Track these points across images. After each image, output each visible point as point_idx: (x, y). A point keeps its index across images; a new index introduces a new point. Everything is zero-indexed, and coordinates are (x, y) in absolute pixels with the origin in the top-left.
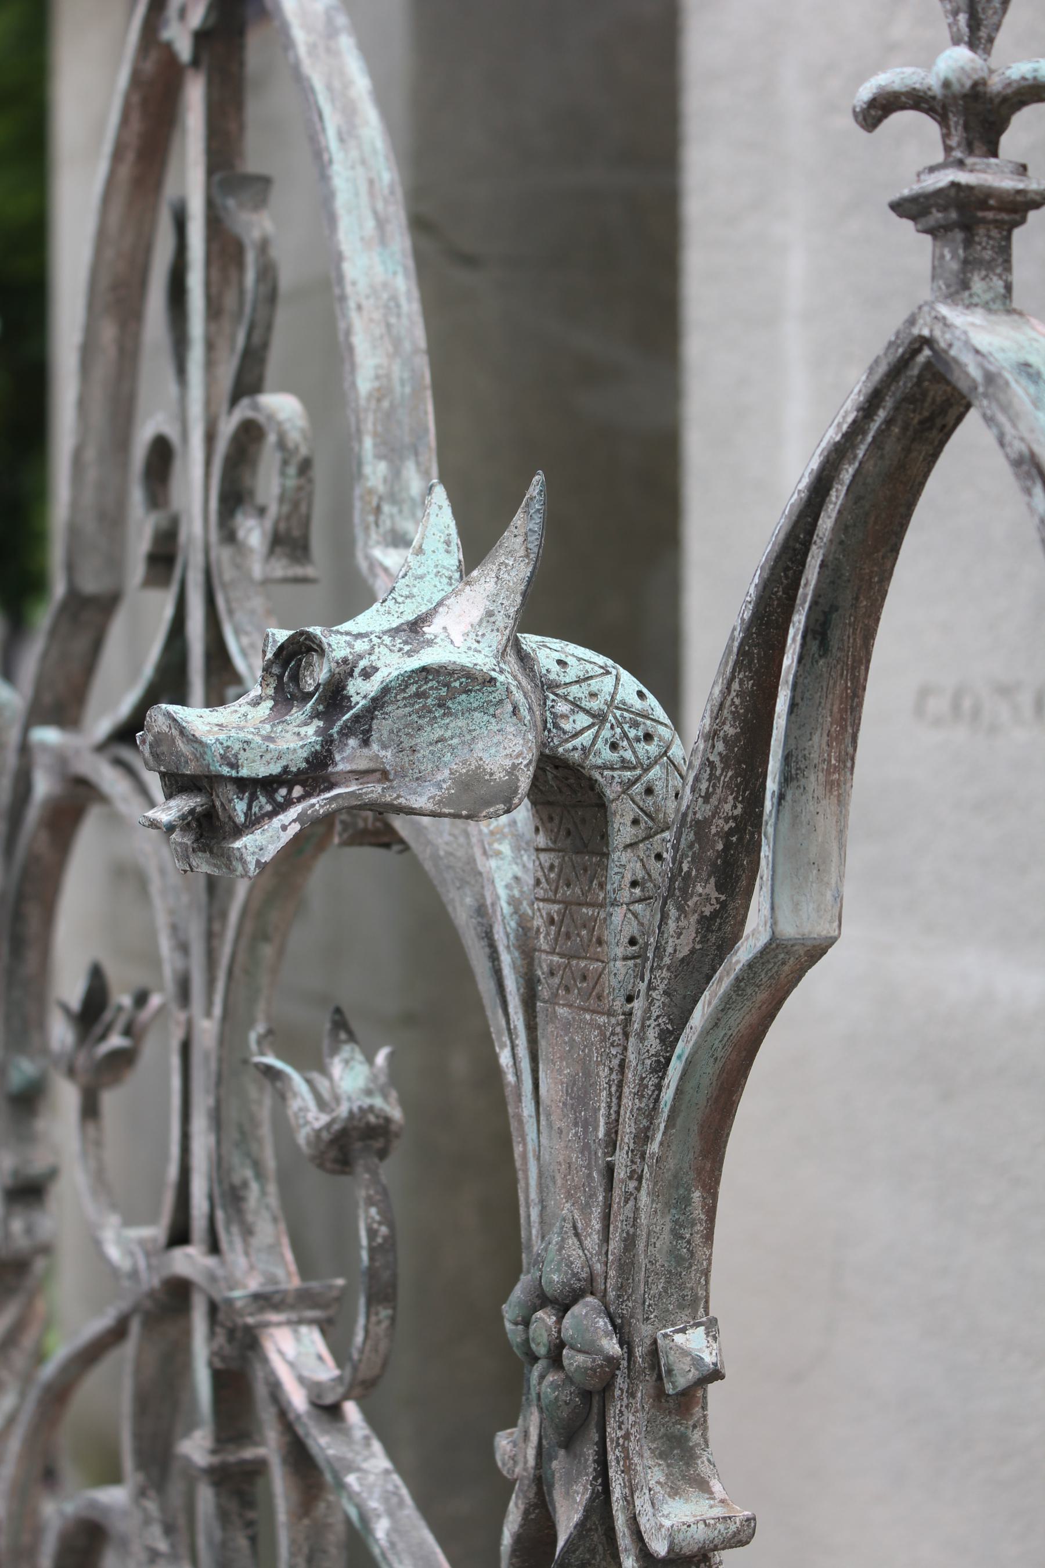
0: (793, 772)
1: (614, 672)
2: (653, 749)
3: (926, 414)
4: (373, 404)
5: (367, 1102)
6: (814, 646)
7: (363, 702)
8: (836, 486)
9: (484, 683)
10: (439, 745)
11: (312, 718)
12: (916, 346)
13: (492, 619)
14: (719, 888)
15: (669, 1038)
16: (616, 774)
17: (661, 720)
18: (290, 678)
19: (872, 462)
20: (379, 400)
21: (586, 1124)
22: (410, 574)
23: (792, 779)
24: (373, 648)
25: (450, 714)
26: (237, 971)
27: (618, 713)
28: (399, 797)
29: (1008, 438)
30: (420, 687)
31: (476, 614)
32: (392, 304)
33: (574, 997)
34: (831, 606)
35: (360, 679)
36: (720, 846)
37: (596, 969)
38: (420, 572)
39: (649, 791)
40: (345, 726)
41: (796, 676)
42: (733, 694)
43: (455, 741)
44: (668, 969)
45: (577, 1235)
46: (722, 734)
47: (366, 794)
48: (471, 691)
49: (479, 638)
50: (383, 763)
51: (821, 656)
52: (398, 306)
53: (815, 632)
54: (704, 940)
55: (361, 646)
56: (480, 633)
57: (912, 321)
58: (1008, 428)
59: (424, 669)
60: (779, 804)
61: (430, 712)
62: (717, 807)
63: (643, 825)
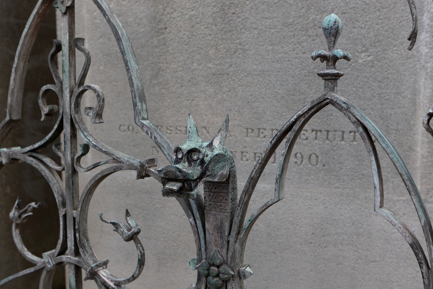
31: (218, 142)
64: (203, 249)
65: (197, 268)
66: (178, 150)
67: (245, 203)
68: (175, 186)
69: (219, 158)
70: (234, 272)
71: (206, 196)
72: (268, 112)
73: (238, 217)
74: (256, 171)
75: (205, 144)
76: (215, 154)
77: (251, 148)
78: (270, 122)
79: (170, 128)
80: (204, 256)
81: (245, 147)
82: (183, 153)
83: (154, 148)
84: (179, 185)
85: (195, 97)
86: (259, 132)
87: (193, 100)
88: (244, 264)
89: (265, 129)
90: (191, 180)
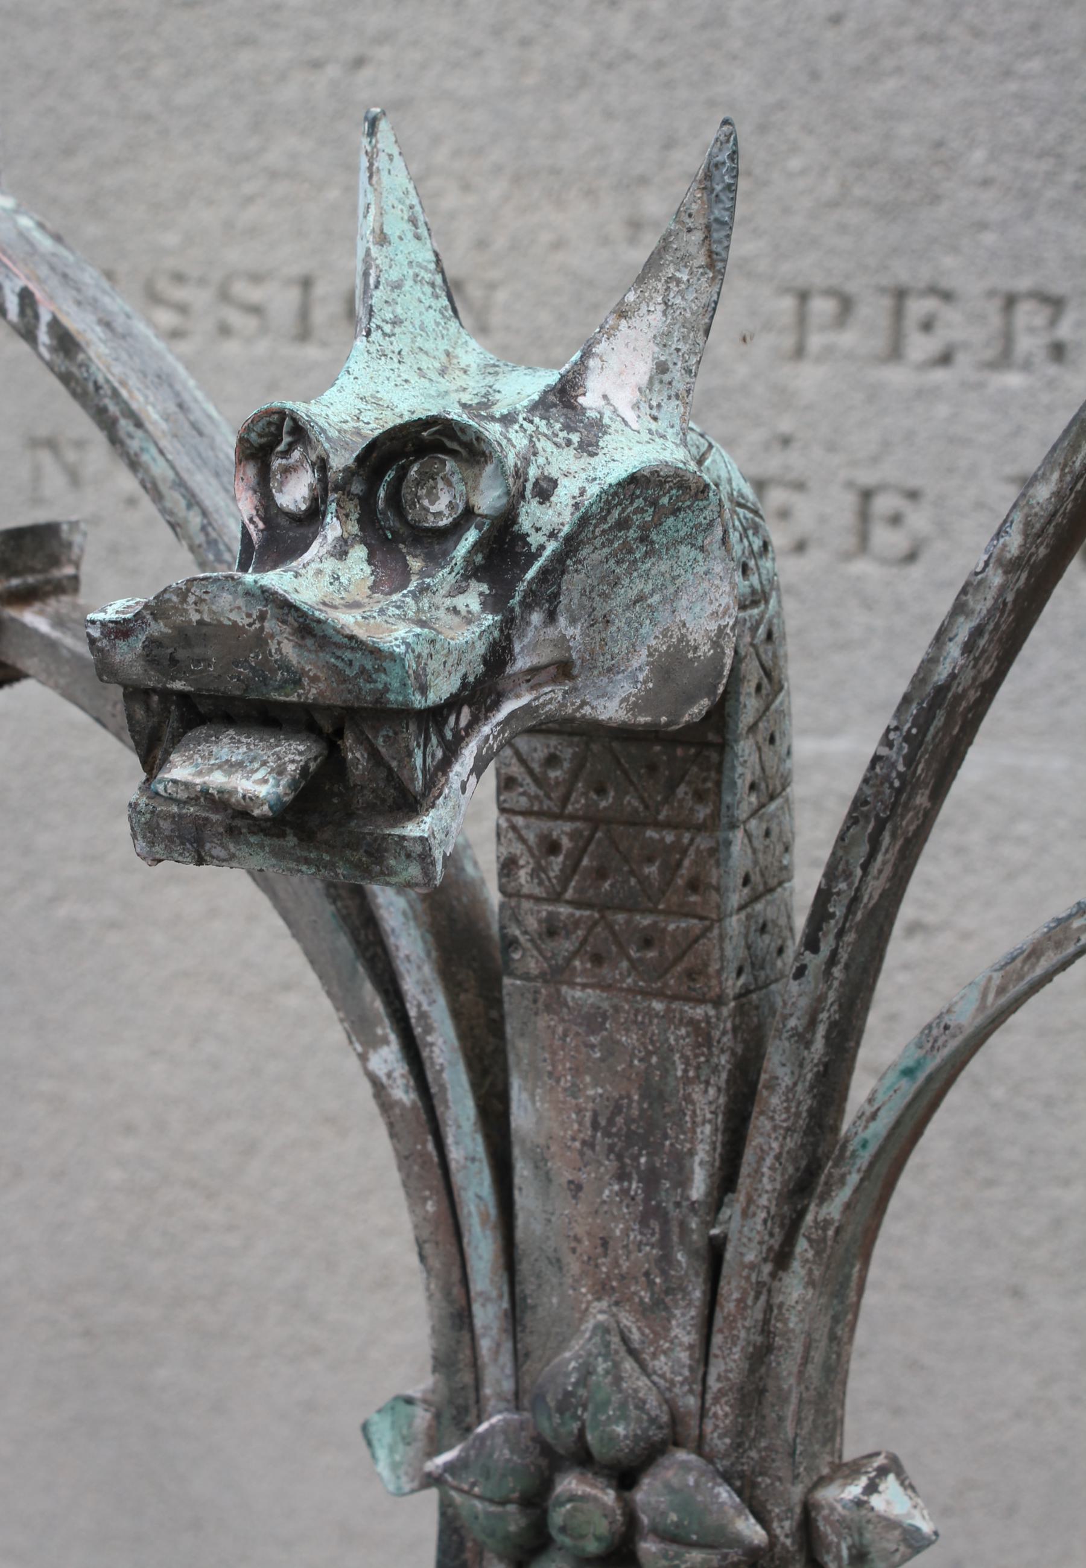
7: (551, 547)
9: (696, 494)
11: (466, 577)
13: (666, 378)
22: (382, 280)
28: (584, 703)
30: (623, 510)
31: (643, 370)
33: (619, 971)
35: (534, 503)
37: (686, 931)
40: (529, 592)
43: (656, 598)
45: (633, 1353)
47: (544, 705)
48: (679, 509)
49: (654, 412)
50: (570, 648)
56: (654, 403)
64: (487, 1316)
65: (431, 1480)
66: (272, 440)
67: (872, 914)
68: (253, 773)
69: (654, 505)
70: (763, 1520)
71: (518, 848)
72: (979, 155)
73: (803, 1038)
74: (977, 632)
75: (523, 386)
76: (618, 473)
77: (831, 447)
78: (989, 238)
79: (179, 294)
80: (497, 1377)
81: (786, 441)
82: (322, 466)
83: (45, 457)
84: (295, 753)
85: (384, 37)
86: (898, 314)
87: (359, 62)
88: (848, 1455)
89: (947, 296)
90: (405, 713)
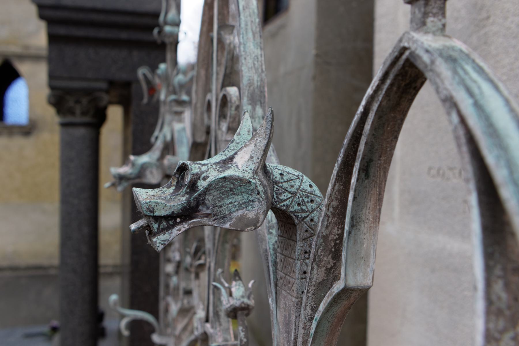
0: (355, 223)
1: (301, 178)
2: (314, 205)
3: (407, 82)
4: (248, 88)
5: (242, 300)
6: (363, 175)
7: (202, 189)
8: (371, 112)
10: (230, 205)
12: (402, 51)
14: (333, 258)
15: (314, 309)
16: (299, 214)
17: (318, 195)
18: (181, 178)
19: (385, 102)
20: (250, 87)
21: (288, 334)
23: (354, 226)
24: (208, 169)
25: (234, 194)
26: (219, 251)
27: (301, 193)
29: (440, 90)
31: (247, 157)
32: (256, 58)
34: (370, 160)
36: (333, 244)
38: (238, 141)
39: (312, 220)
41: (356, 187)
42: (335, 190)
44: (314, 286)
46: (332, 205)
51: (366, 179)
52: (258, 58)
53: (363, 170)
54: (328, 276)
55: (204, 168)
57: (400, 40)
58: (440, 84)
59: (224, 178)
60: (349, 235)
61: (227, 193)
62: (331, 231)
63: (309, 232)
